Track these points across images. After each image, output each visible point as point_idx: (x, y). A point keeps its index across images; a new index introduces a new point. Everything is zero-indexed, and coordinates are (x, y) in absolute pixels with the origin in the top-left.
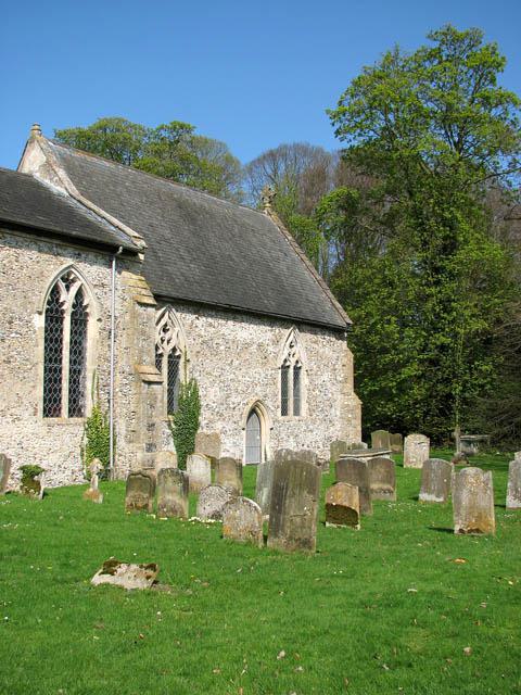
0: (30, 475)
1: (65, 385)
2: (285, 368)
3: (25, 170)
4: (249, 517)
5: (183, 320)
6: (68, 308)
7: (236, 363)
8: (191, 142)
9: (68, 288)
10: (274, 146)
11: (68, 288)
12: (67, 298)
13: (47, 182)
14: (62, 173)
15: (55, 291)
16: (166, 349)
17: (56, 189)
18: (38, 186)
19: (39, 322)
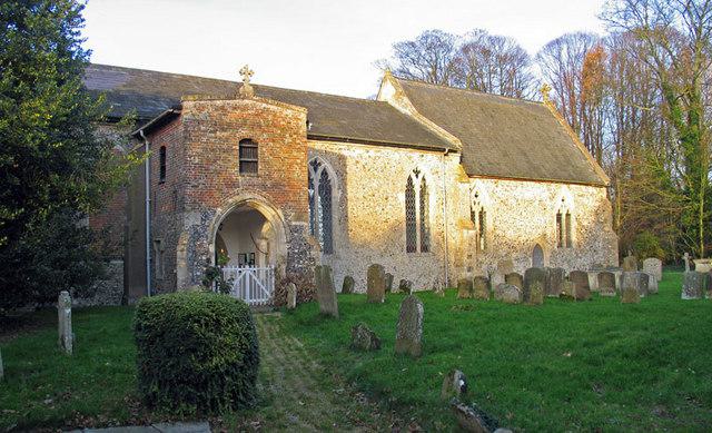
0: (405, 287)
1: (418, 233)
2: (559, 216)
3: (382, 99)
4: (513, 294)
5: (482, 185)
6: (417, 190)
7: (524, 214)
8: (450, 375)
9: (417, 176)
10: (557, 35)
11: (417, 176)
12: (417, 183)
13: (397, 106)
14: (406, 100)
15: (410, 179)
16: (477, 210)
17: (403, 111)
18: (392, 109)
19: (402, 197)
